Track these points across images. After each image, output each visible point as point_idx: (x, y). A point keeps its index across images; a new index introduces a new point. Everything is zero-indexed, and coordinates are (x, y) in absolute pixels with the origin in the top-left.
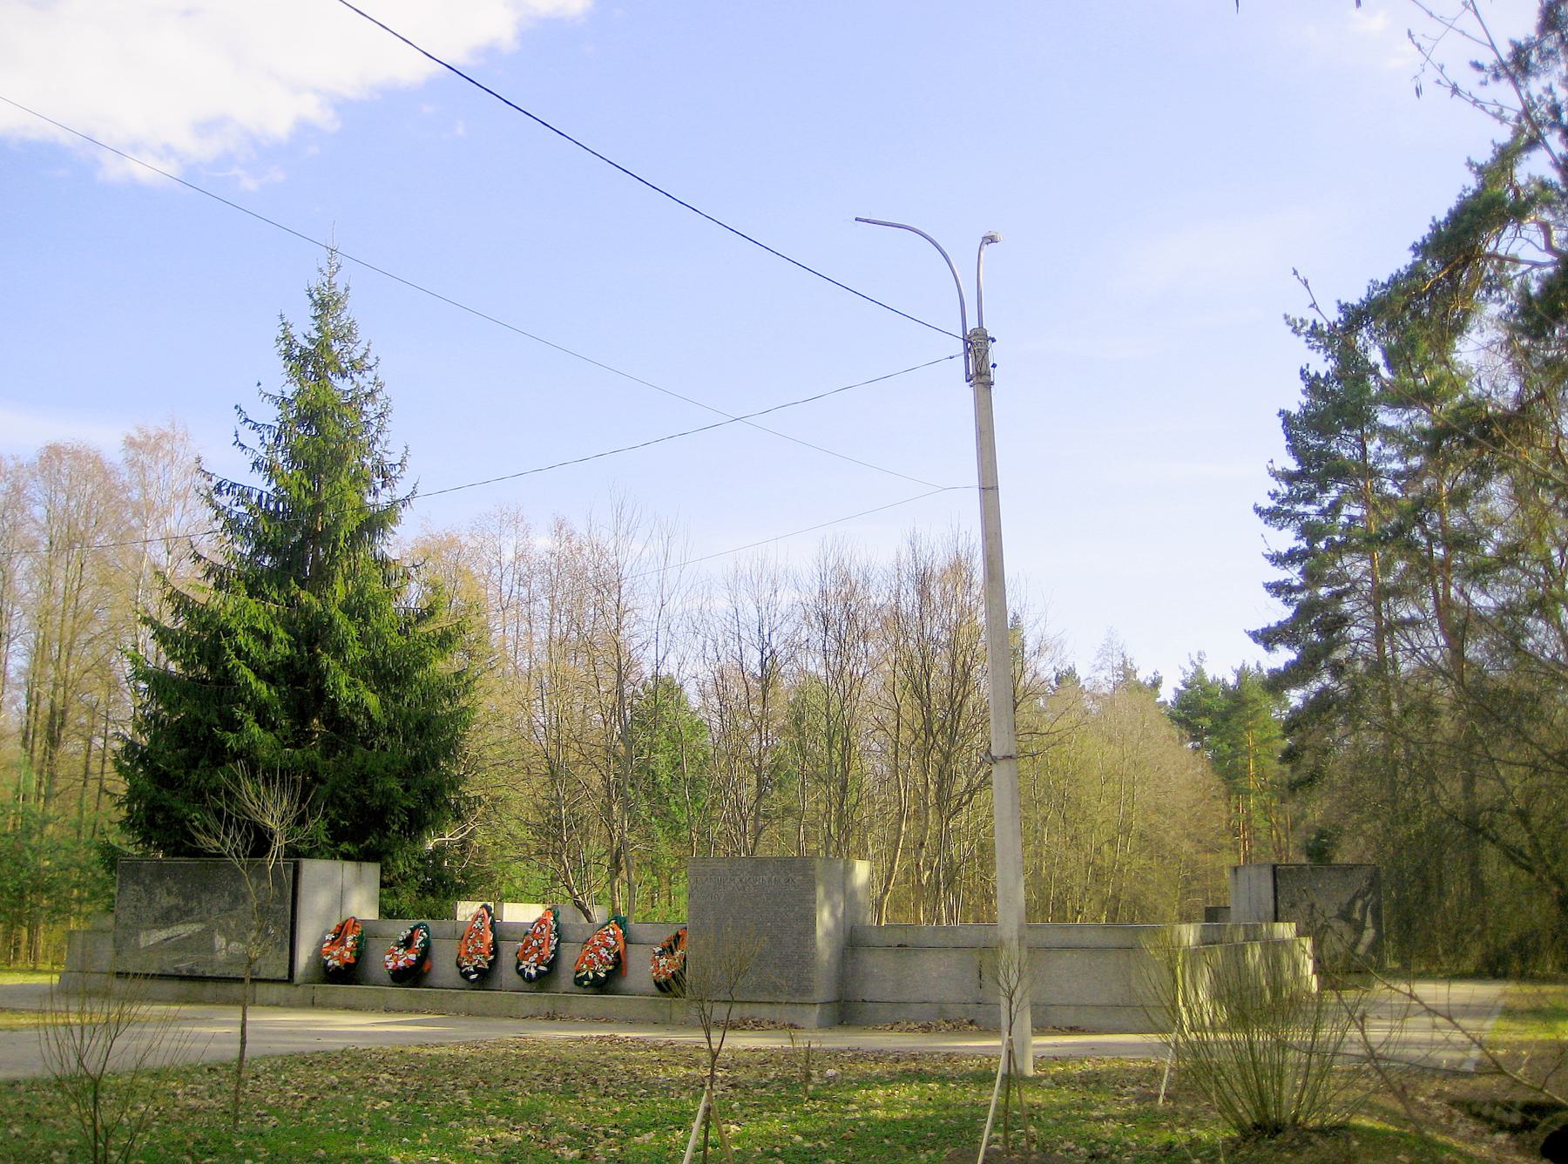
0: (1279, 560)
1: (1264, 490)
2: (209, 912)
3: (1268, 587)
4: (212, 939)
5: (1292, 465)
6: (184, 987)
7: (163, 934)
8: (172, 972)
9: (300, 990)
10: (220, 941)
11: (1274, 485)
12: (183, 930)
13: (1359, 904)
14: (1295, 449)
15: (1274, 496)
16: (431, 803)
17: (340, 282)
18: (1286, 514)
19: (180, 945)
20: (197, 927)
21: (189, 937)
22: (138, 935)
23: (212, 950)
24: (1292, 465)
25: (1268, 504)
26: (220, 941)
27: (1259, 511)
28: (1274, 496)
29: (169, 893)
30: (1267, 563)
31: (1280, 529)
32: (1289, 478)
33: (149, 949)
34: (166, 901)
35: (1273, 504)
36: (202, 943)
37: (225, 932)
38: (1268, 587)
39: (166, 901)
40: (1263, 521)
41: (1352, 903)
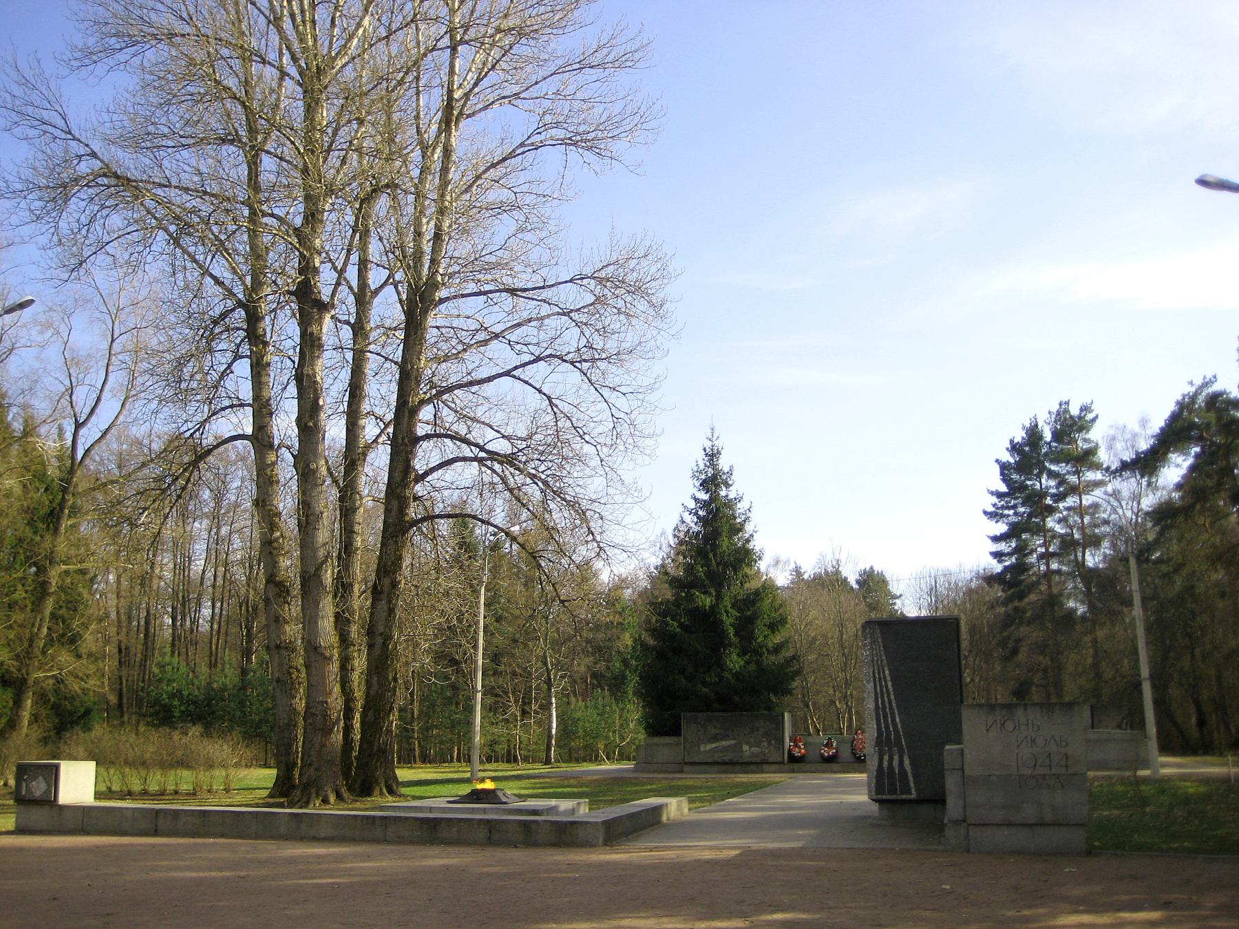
0: (996, 539)
1: (989, 502)
2: (738, 735)
3: (992, 554)
4: (742, 748)
5: (1003, 488)
6: (723, 768)
7: (714, 745)
8: (719, 760)
9: (786, 766)
10: (745, 748)
11: (995, 500)
12: (725, 743)
13: (1125, 721)
14: (1005, 479)
15: (994, 505)
16: (137, 727)
17: (718, 443)
18: (1002, 516)
19: (725, 749)
20: (732, 742)
21: (729, 746)
22: (699, 746)
23: (742, 751)
24: (1003, 488)
25: (991, 509)
26: (745, 748)
27: (985, 513)
28: (994, 505)
29: (715, 727)
30: (989, 541)
31: (997, 522)
32: (1000, 495)
33: (706, 752)
34: (714, 731)
35: (993, 509)
36: (737, 746)
37: (747, 743)
38: (992, 554)
39: (714, 731)
40: (994, 522)
41: (1122, 722)
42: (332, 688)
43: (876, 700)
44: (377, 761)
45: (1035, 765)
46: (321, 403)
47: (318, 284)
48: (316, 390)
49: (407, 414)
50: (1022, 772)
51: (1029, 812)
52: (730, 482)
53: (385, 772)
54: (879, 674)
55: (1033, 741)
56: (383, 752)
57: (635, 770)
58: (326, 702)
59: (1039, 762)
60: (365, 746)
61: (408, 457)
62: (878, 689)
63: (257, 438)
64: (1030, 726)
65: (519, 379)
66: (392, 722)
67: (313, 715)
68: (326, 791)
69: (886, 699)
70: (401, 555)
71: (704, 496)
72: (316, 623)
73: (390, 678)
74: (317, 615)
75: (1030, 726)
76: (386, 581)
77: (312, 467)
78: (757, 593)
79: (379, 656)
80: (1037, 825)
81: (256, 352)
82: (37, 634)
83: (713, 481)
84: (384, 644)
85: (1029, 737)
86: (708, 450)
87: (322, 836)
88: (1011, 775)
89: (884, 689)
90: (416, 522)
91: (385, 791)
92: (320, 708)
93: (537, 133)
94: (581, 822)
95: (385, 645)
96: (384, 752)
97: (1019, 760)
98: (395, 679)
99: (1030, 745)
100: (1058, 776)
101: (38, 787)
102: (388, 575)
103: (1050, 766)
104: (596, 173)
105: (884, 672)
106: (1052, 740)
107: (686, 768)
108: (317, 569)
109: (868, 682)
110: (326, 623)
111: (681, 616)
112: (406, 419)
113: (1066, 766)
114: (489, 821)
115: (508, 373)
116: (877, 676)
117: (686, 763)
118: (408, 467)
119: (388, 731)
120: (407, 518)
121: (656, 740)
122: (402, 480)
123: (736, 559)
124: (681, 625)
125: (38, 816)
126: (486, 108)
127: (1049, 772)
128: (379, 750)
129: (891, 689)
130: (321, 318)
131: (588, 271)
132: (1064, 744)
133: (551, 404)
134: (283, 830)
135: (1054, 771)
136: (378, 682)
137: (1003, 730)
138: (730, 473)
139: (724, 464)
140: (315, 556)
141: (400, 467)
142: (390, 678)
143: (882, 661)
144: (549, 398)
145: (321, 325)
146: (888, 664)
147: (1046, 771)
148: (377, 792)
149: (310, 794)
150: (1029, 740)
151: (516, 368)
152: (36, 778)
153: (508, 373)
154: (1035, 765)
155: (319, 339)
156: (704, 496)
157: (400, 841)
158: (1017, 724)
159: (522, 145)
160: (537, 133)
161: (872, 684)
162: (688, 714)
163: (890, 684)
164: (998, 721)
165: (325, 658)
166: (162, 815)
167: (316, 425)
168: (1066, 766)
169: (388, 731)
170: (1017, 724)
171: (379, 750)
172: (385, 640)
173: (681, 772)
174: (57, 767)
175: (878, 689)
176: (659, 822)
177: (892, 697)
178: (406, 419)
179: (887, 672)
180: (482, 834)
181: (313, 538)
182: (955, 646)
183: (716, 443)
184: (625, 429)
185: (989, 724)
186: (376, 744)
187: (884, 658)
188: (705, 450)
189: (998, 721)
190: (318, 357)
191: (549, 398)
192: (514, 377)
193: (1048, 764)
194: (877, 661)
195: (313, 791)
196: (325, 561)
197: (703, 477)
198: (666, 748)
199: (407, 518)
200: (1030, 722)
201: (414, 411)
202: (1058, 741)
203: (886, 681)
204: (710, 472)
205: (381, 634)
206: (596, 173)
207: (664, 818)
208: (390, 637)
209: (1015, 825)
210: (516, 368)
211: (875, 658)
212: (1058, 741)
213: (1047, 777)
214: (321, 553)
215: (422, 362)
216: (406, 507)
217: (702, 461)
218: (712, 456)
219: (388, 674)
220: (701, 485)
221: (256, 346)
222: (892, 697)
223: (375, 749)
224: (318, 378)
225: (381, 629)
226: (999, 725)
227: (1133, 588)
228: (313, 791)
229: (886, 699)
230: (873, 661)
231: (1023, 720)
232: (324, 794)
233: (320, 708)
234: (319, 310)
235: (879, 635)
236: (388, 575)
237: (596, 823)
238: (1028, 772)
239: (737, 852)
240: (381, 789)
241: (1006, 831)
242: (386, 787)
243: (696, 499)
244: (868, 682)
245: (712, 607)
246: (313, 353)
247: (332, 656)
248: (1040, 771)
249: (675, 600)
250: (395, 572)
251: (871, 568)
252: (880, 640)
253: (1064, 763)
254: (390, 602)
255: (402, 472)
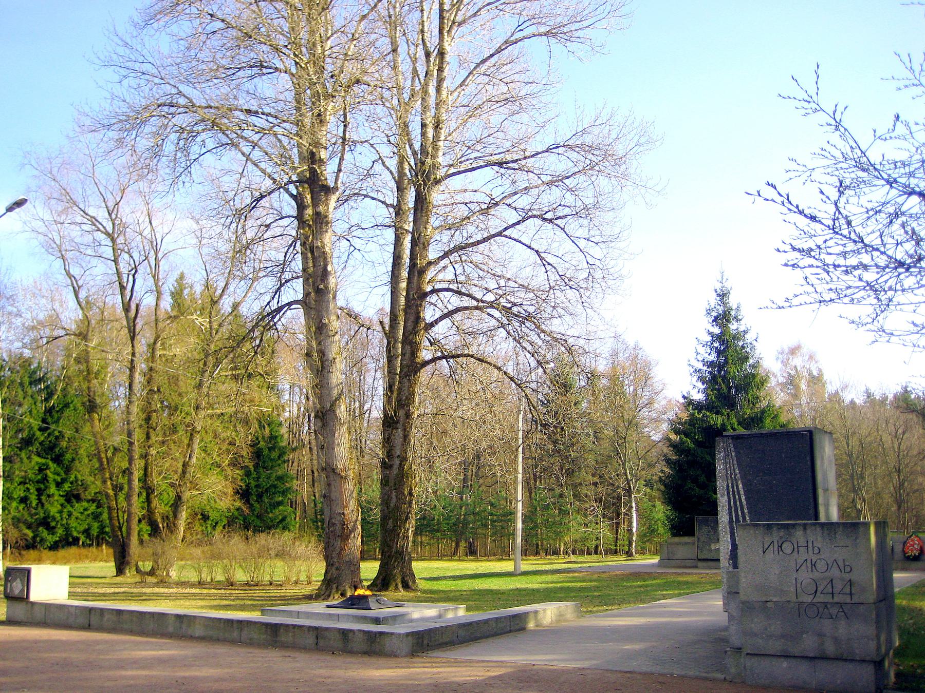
17: (728, 285)
42: (349, 502)
43: (730, 514)
44: (395, 561)
45: (816, 592)
46: (329, 268)
47: (324, 172)
48: (325, 259)
49: (416, 274)
50: (800, 600)
51: (809, 644)
52: (740, 317)
53: (401, 571)
54: (733, 487)
55: (814, 565)
56: (400, 554)
57: (660, 565)
58: (343, 514)
59: (820, 589)
60: (386, 549)
61: (418, 310)
62: (732, 503)
63: (305, 303)
64: (810, 549)
65: (510, 238)
66: (408, 529)
67: (334, 524)
68: (345, 586)
69: (740, 513)
70: (413, 391)
71: (717, 330)
72: (333, 449)
73: (406, 493)
74: (334, 442)
75: (810, 549)
76: (402, 413)
77: (324, 322)
78: (763, 412)
79: (397, 475)
80: (837, 659)
81: (303, 234)
82: (188, 462)
83: (723, 318)
84: (401, 464)
85: (809, 561)
86: (719, 291)
87: (197, 635)
88: (789, 602)
89: (738, 503)
90: (426, 363)
91: (400, 586)
92: (338, 518)
93: (520, 30)
94: (388, 633)
95: (401, 466)
96: (401, 553)
97: (799, 585)
98: (411, 494)
99: (810, 569)
100: (841, 605)
101: (17, 587)
102: (403, 408)
103: (833, 594)
104: (580, 59)
105: (737, 486)
106: (835, 563)
107: (700, 564)
108: (332, 405)
109: (722, 496)
110: (342, 450)
111: (695, 433)
112: (416, 278)
113: (851, 594)
114: (316, 629)
115: (499, 234)
116: (731, 489)
117: (700, 560)
118: (418, 319)
119: (404, 536)
120: (418, 360)
121: (677, 539)
122: (414, 329)
123: (78, 361)
124: (696, 442)
125: (20, 610)
126: (475, 15)
127: (831, 601)
128: (397, 552)
129: (744, 503)
130: (327, 199)
131: (560, 141)
132: (848, 569)
133: (542, 259)
134: (171, 629)
135: (836, 599)
136: (396, 496)
137: (781, 553)
138: (738, 309)
139: (733, 301)
140: (329, 395)
141: (412, 318)
142: (406, 493)
143: (735, 475)
144: (537, 251)
145: (327, 205)
146: (742, 478)
147: (828, 599)
148: (392, 587)
149: (331, 589)
150: (809, 565)
151: (506, 229)
152: (15, 579)
153: (499, 234)
154: (816, 592)
155: (326, 217)
156: (717, 330)
157: (250, 643)
158: (796, 546)
159: (506, 42)
160: (520, 30)
161: (726, 497)
162: (700, 518)
163: (743, 498)
164: (776, 543)
165: (342, 477)
166: (93, 612)
167: (326, 287)
168: (851, 594)
169: (404, 536)
170: (796, 546)
171: (397, 552)
172: (402, 461)
173: (696, 567)
174: (28, 572)
175: (732, 503)
176: (523, 629)
177: (746, 511)
178: (416, 278)
179: (740, 486)
180: (310, 640)
181: (328, 380)
182: (808, 458)
183: (725, 284)
184: (598, 274)
185: (766, 546)
186: (394, 546)
187: (737, 471)
188: (716, 291)
189: (776, 543)
190: (326, 231)
191: (537, 251)
192: (506, 236)
193: (848, 592)
194: (731, 474)
195: (334, 586)
196: (338, 399)
197: (714, 314)
198: (685, 547)
199: (418, 360)
200: (810, 545)
201: (422, 272)
202: (841, 564)
203: (739, 495)
204: (721, 309)
205: (399, 456)
206: (580, 59)
207: (531, 625)
208: (405, 459)
209: (795, 657)
210: (506, 229)
211: (729, 472)
212: (841, 564)
213: (829, 606)
214: (335, 392)
215: (429, 230)
216: (417, 351)
217: (713, 300)
218: (723, 296)
219: (404, 490)
220: (713, 321)
221: (303, 229)
222: (746, 511)
223: (394, 550)
224: (327, 249)
225: (398, 453)
226: (776, 546)
227: (372, 373)
228: (334, 586)
229: (740, 513)
230: (727, 474)
231: (802, 542)
232: (343, 588)
233: (338, 518)
234: (326, 193)
235: (732, 449)
236: (403, 408)
237: (400, 634)
238: (809, 599)
239: (512, 670)
240: (396, 585)
241: (785, 664)
242: (402, 582)
243: (709, 333)
244: (722, 496)
245: (723, 425)
246: (321, 228)
247: (347, 476)
248: (820, 598)
249: (690, 420)
250: (408, 406)
251: (906, 391)
252: (733, 454)
253: (847, 590)
254: (405, 430)
255: (413, 322)
